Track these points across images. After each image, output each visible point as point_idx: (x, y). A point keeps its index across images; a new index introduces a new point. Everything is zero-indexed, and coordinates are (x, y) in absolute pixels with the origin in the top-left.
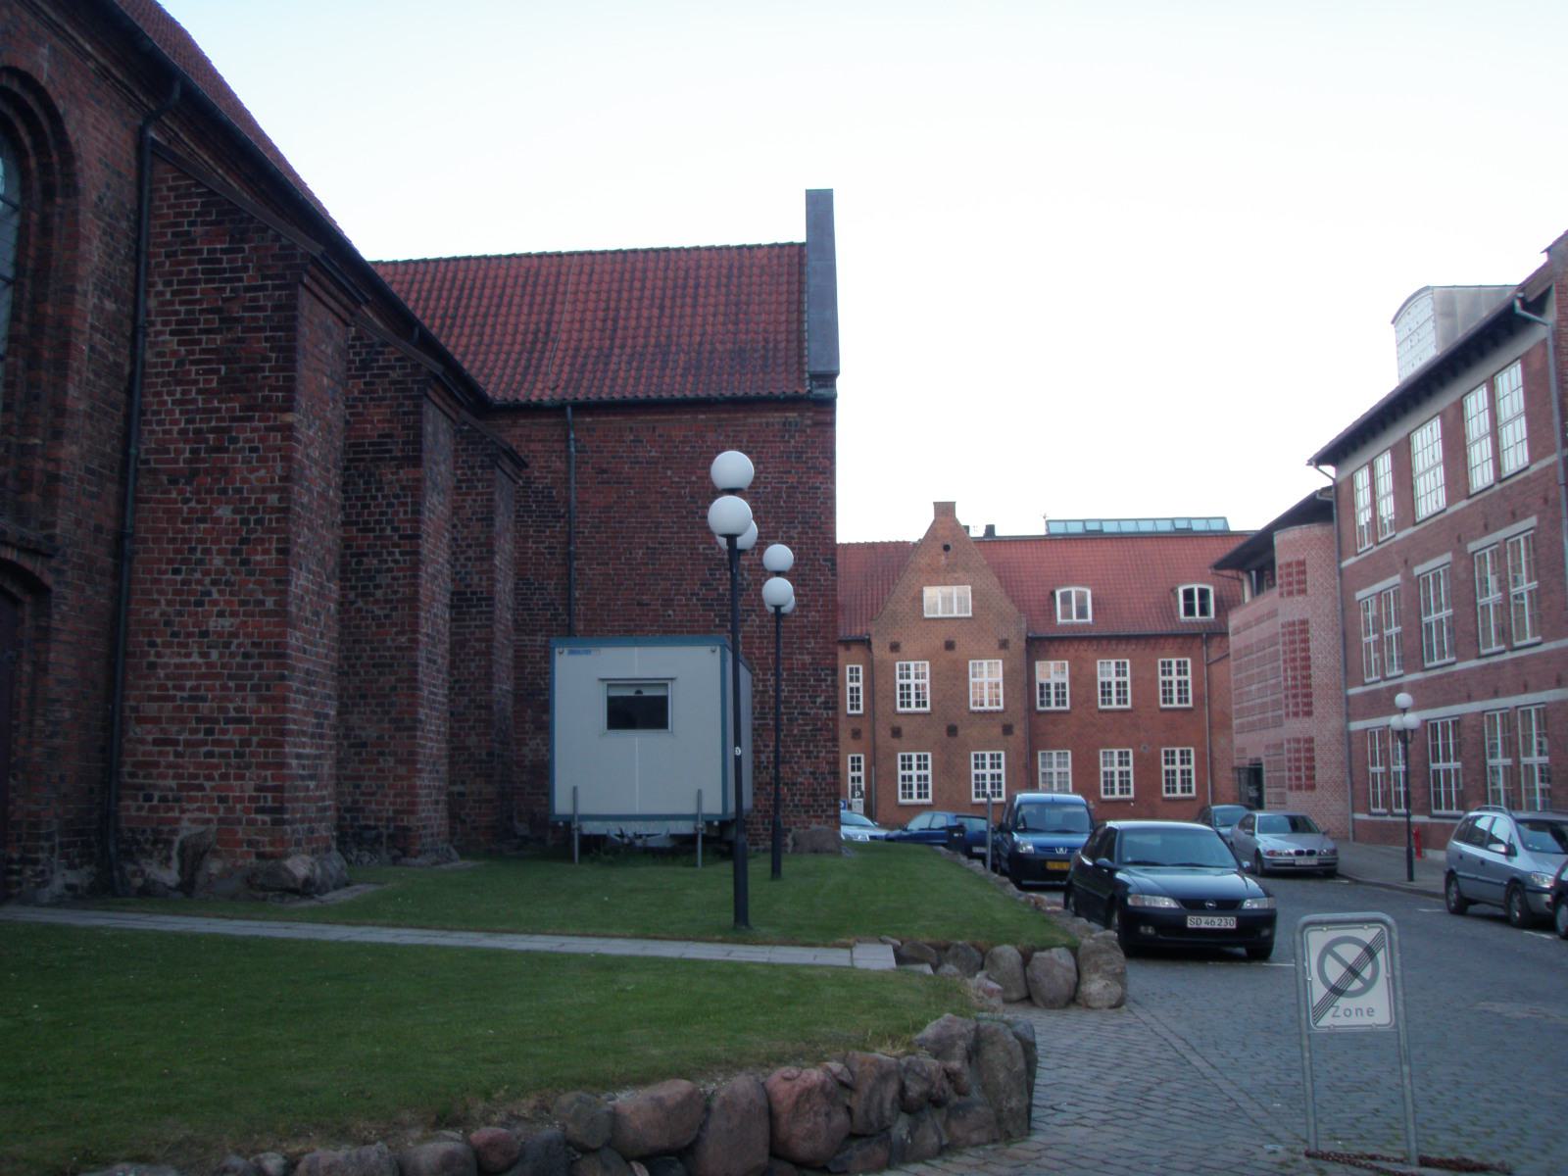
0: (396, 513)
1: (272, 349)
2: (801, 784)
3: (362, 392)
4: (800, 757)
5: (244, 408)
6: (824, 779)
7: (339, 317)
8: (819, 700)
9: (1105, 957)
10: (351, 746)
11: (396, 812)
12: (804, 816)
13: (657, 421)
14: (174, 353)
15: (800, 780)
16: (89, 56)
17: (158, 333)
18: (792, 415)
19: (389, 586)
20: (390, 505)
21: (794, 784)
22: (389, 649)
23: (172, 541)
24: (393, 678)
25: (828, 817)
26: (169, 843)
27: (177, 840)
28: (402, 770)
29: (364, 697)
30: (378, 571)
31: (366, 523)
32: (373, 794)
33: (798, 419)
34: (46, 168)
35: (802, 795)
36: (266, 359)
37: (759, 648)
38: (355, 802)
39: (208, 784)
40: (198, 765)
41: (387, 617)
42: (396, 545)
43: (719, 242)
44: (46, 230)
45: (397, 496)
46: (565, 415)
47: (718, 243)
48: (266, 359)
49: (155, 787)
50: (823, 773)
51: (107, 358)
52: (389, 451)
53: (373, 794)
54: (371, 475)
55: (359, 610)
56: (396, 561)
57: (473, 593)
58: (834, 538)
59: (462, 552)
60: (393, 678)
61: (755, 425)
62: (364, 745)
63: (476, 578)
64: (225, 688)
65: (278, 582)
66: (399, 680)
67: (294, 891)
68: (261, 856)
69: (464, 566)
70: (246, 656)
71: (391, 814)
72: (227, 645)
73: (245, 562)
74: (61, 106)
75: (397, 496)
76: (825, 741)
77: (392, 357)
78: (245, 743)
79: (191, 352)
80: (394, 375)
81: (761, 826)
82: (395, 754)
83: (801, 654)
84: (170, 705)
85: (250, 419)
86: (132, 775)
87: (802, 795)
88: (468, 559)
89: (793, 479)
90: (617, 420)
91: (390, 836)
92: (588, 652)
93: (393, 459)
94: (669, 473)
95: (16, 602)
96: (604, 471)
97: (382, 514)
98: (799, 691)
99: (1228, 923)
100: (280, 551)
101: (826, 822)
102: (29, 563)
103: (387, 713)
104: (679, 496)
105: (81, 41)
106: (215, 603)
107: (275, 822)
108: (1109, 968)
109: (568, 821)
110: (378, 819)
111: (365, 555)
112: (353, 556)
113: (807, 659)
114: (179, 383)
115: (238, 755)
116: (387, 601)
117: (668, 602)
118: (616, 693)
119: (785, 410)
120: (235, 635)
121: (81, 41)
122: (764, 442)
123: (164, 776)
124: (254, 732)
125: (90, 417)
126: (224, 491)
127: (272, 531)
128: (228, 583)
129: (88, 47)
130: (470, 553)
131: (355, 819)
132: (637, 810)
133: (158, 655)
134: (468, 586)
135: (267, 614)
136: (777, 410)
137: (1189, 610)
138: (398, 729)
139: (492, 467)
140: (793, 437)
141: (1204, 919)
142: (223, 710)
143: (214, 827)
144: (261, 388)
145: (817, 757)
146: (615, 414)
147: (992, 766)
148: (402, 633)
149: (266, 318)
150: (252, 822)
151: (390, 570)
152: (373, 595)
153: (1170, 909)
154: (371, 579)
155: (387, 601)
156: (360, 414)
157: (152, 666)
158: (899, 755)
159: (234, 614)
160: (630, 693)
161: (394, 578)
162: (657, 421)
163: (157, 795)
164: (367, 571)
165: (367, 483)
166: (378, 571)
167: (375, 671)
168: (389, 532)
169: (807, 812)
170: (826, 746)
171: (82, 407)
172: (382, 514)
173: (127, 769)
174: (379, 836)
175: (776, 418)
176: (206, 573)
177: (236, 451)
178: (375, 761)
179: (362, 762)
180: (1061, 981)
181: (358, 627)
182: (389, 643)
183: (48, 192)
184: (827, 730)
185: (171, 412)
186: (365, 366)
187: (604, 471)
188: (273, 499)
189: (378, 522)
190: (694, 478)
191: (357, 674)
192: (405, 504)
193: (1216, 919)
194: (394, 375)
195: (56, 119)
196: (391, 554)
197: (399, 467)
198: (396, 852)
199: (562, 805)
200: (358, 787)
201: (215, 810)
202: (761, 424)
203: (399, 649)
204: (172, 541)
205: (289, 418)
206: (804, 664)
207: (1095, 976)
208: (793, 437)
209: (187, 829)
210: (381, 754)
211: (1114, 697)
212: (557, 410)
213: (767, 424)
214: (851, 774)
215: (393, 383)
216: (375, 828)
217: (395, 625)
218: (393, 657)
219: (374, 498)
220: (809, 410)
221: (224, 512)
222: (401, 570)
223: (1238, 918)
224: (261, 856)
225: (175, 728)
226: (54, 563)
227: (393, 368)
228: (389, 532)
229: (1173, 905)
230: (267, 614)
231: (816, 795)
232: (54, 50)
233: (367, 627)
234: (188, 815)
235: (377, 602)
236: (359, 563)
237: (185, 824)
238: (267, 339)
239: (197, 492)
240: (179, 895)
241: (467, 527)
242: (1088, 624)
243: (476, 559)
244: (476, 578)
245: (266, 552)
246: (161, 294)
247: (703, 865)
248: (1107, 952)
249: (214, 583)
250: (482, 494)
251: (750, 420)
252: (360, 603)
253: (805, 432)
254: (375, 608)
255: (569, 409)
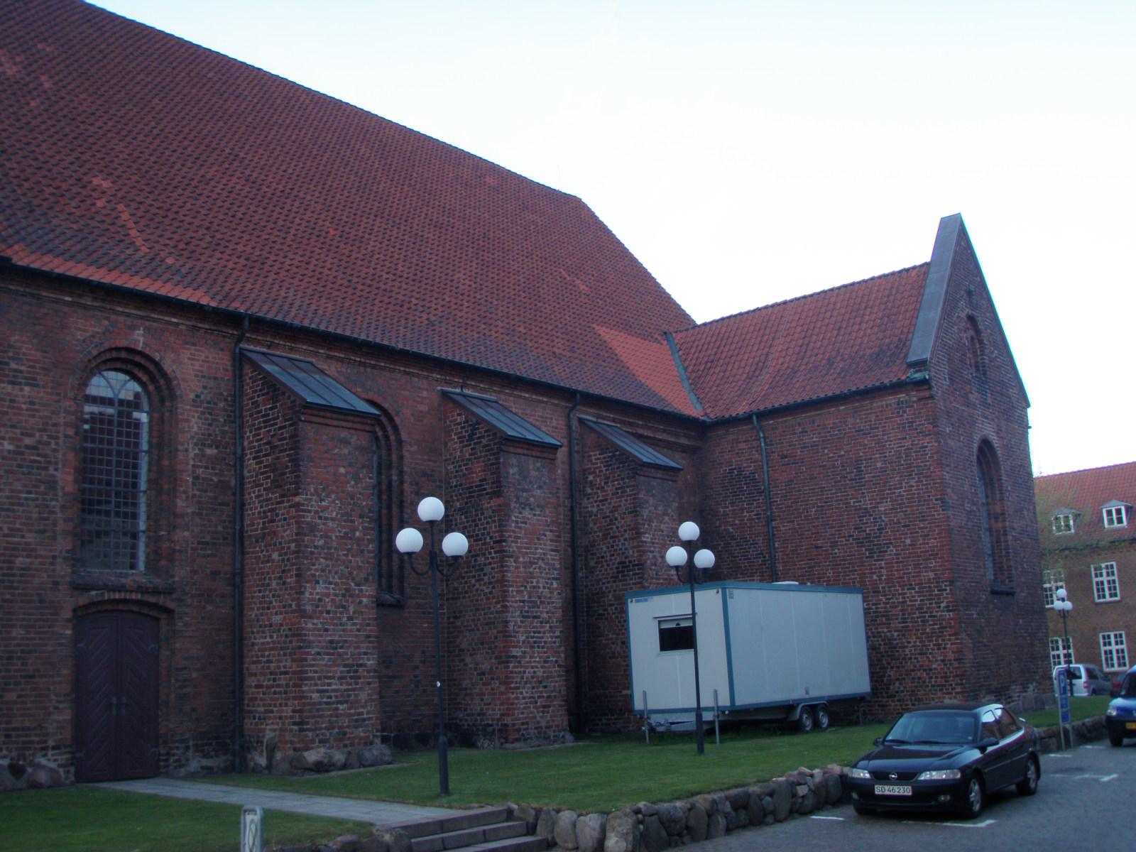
0: (491, 528)
1: (289, 461)
2: (935, 669)
3: (471, 455)
4: (933, 649)
5: (282, 496)
6: (951, 664)
7: (356, 429)
8: (943, 605)
9: (618, 821)
10: (478, 674)
11: (501, 715)
12: (939, 694)
13: (814, 416)
14: (254, 470)
15: (934, 666)
16: (177, 324)
17: (249, 459)
18: (902, 396)
19: (490, 573)
20: (488, 523)
21: (931, 670)
22: (492, 613)
23: (258, 574)
24: (495, 631)
25: (957, 693)
26: (262, 742)
27: (265, 740)
28: (503, 688)
29: (482, 644)
30: (485, 565)
31: (477, 535)
32: (490, 704)
33: (907, 398)
34: (158, 388)
35: (936, 677)
36: (287, 467)
37: (897, 571)
38: (482, 709)
39: (275, 709)
40: (272, 699)
41: (491, 593)
42: (492, 548)
43: (887, 270)
44: (162, 420)
45: (490, 517)
46: (752, 423)
47: (887, 271)
48: (287, 467)
49: (256, 711)
50: (950, 660)
51: (211, 480)
52: (485, 489)
53: (490, 704)
54: (478, 505)
55: (477, 590)
56: (492, 558)
57: (630, 562)
58: (1030, 474)
59: (622, 535)
60: (495, 631)
61: (878, 407)
62: (483, 674)
63: (631, 552)
64: (279, 655)
65: (297, 593)
66: (498, 632)
67: (310, 770)
68: (295, 749)
69: (623, 544)
70: (287, 636)
71: (499, 716)
72: (279, 631)
73: (284, 583)
74: (157, 357)
75: (490, 517)
76: (950, 635)
77: (482, 430)
78: (287, 685)
79: (260, 468)
80: (484, 441)
81: (909, 703)
82: (498, 678)
83: (926, 572)
84: (260, 666)
85: (283, 502)
86: (248, 706)
87: (936, 677)
88: (625, 540)
89: (908, 444)
90: (790, 419)
91: (499, 730)
92: (646, 600)
93: (487, 494)
94: (826, 451)
95: (157, 619)
96: (786, 457)
97: (485, 529)
98: (928, 600)
99: (905, 790)
100: (297, 575)
101: (955, 697)
102: (161, 600)
103: (493, 653)
104: (834, 466)
105: (166, 318)
106: (274, 607)
107: (301, 730)
108: (620, 829)
109: (641, 712)
110: (493, 720)
111: (478, 555)
112: (472, 556)
113: (931, 575)
114: (257, 486)
115: (286, 692)
116: (491, 583)
117: (834, 544)
118: (664, 626)
119: (896, 393)
120: (281, 625)
121: (166, 318)
122: (886, 418)
123: (259, 705)
124: (290, 679)
125: (199, 514)
126: (275, 544)
127: (293, 564)
128: (278, 596)
129: (174, 320)
130: (626, 536)
131: (482, 720)
132: (680, 706)
133: (255, 639)
134: (626, 557)
135: (293, 612)
136: (890, 395)
137: (1111, 521)
138: (499, 663)
139: (634, 477)
140: (904, 412)
141: (887, 787)
142: (279, 667)
143: (277, 733)
144: (285, 485)
145: (945, 648)
146: (786, 416)
147: (1117, 643)
148: (497, 603)
149: (287, 444)
150: (291, 730)
151: (490, 563)
152: (483, 580)
153: (865, 779)
154: (482, 570)
155: (491, 583)
156: (470, 469)
157: (253, 644)
158: (1101, 635)
159: (281, 613)
160: (673, 625)
161: (493, 569)
162: (814, 416)
163: (257, 715)
164: (480, 565)
165: (476, 510)
166: (485, 565)
167: (486, 627)
168: (488, 540)
169: (941, 690)
170: (950, 640)
171: (190, 510)
172: (485, 529)
173: (246, 702)
174: (494, 730)
175: (891, 400)
176: (270, 591)
177: (279, 521)
178: (490, 684)
179: (484, 684)
180: (588, 837)
181: (477, 600)
182: (492, 609)
183: (162, 401)
184: (950, 627)
185: (254, 503)
186: (471, 438)
187: (786, 457)
188: (293, 546)
189: (483, 534)
190: (842, 453)
191: (478, 630)
192: (494, 521)
193: (896, 788)
194: (484, 441)
195: (157, 364)
196: (490, 553)
197: (491, 498)
198: (503, 740)
199: (638, 704)
200: (482, 700)
201: (278, 724)
202: (882, 406)
203: (497, 612)
204: (258, 574)
205: (297, 499)
206: (929, 579)
207: (612, 835)
208: (904, 412)
209: (269, 735)
210: (492, 679)
211: (1107, 593)
212: (747, 419)
213: (887, 405)
214: (1124, 646)
215: (485, 446)
216: (492, 725)
217: (494, 598)
218: (495, 618)
219: (480, 519)
220: (912, 390)
221: (275, 556)
222: (495, 563)
223: (913, 788)
224: (295, 749)
225: (262, 678)
226: (174, 596)
227: (483, 437)
228: (488, 540)
229: (868, 776)
230: (293, 612)
231: (946, 677)
232: (147, 329)
233: (482, 600)
234: (268, 727)
235: (485, 584)
236: (475, 561)
237: (268, 732)
238: (288, 456)
239: (265, 546)
240: (266, 772)
241: (623, 518)
242: (1123, 528)
243: (631, 539)
244: (631, 552)
245: (291, 577)
246: (248, 437)
247: (721, 742)
248: (621, 818)
249: (274, 596)
250: (630, 495)
251: (875, 405)
252: (477, 586)
253: (912, 406)
254: (484, 588)
255: (754, 418)
